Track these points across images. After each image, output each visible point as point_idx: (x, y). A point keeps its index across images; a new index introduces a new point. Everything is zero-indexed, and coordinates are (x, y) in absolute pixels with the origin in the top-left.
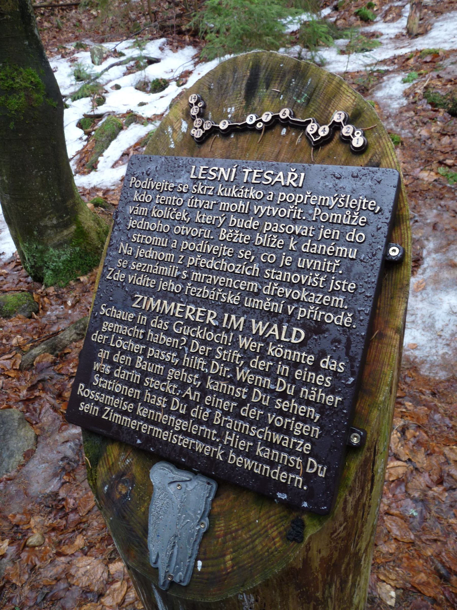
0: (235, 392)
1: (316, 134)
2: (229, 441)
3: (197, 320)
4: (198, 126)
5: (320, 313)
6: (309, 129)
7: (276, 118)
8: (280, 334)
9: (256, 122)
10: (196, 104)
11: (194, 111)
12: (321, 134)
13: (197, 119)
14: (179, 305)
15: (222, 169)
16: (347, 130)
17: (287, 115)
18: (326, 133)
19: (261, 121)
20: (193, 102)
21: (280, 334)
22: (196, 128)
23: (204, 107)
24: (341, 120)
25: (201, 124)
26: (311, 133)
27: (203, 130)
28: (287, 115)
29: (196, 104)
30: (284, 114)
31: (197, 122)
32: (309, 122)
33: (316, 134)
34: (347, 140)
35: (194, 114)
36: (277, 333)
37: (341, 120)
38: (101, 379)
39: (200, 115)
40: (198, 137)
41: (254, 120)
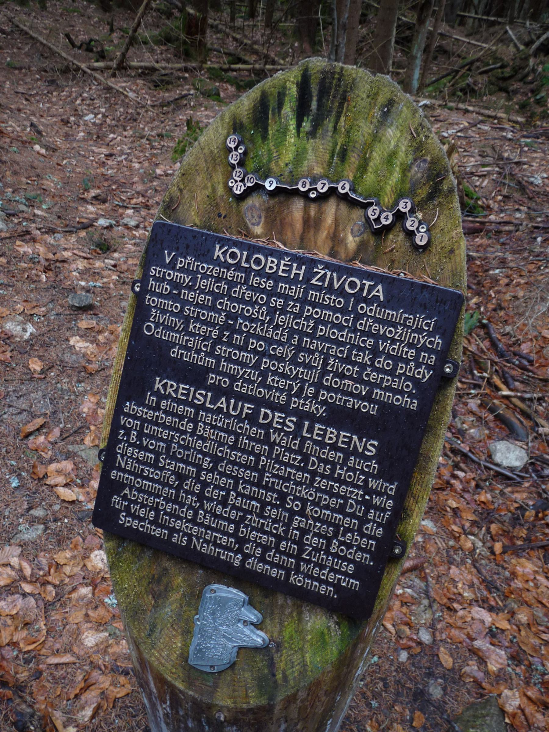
0: (266, 496)
1: (377, 220)
2: (341, 469)
3: (179, 396)
4: (239, 179)
5: (404, 315)
6: (370, 211)
7: (333, 191)
8: (228, 407)
9: (310, 190)
10: (236, 149)
11: (233, 159)
12: (384, 222)
13: (238, 170)
14: (283, 262)
15: (355, 438)
16: (410, 224)
17: (347, 190)
18: (389, 222)
19: (316, 189)
20: (232, 145)
21: (228, 407)
22: (236, 181)
23: (245, 153)
24: (406, 210)
25: (242, 176)
26: (372, 218)
27: (245, 185)
28: (347, 190)
29: (236, 149)
30: (343, 188)
31: (237, 174)
32: (371, 204)
33: (377, 220)
34: (411, 235)
35: (233, 162)
36: (224, 406)
37: (406, 210)
38: (168, 461)
39: (241, 164)
40: (238, 192)
41: (308, 187)
